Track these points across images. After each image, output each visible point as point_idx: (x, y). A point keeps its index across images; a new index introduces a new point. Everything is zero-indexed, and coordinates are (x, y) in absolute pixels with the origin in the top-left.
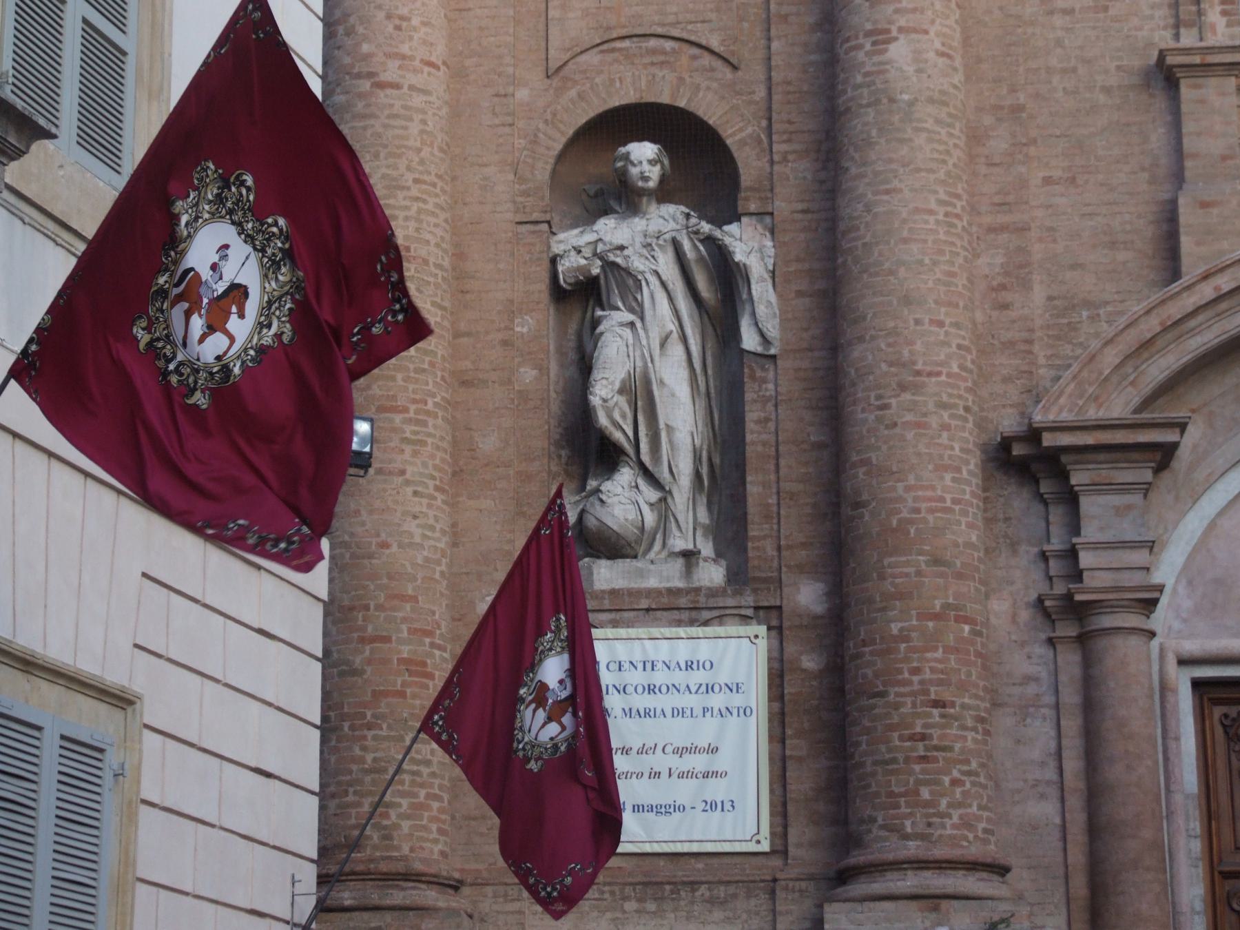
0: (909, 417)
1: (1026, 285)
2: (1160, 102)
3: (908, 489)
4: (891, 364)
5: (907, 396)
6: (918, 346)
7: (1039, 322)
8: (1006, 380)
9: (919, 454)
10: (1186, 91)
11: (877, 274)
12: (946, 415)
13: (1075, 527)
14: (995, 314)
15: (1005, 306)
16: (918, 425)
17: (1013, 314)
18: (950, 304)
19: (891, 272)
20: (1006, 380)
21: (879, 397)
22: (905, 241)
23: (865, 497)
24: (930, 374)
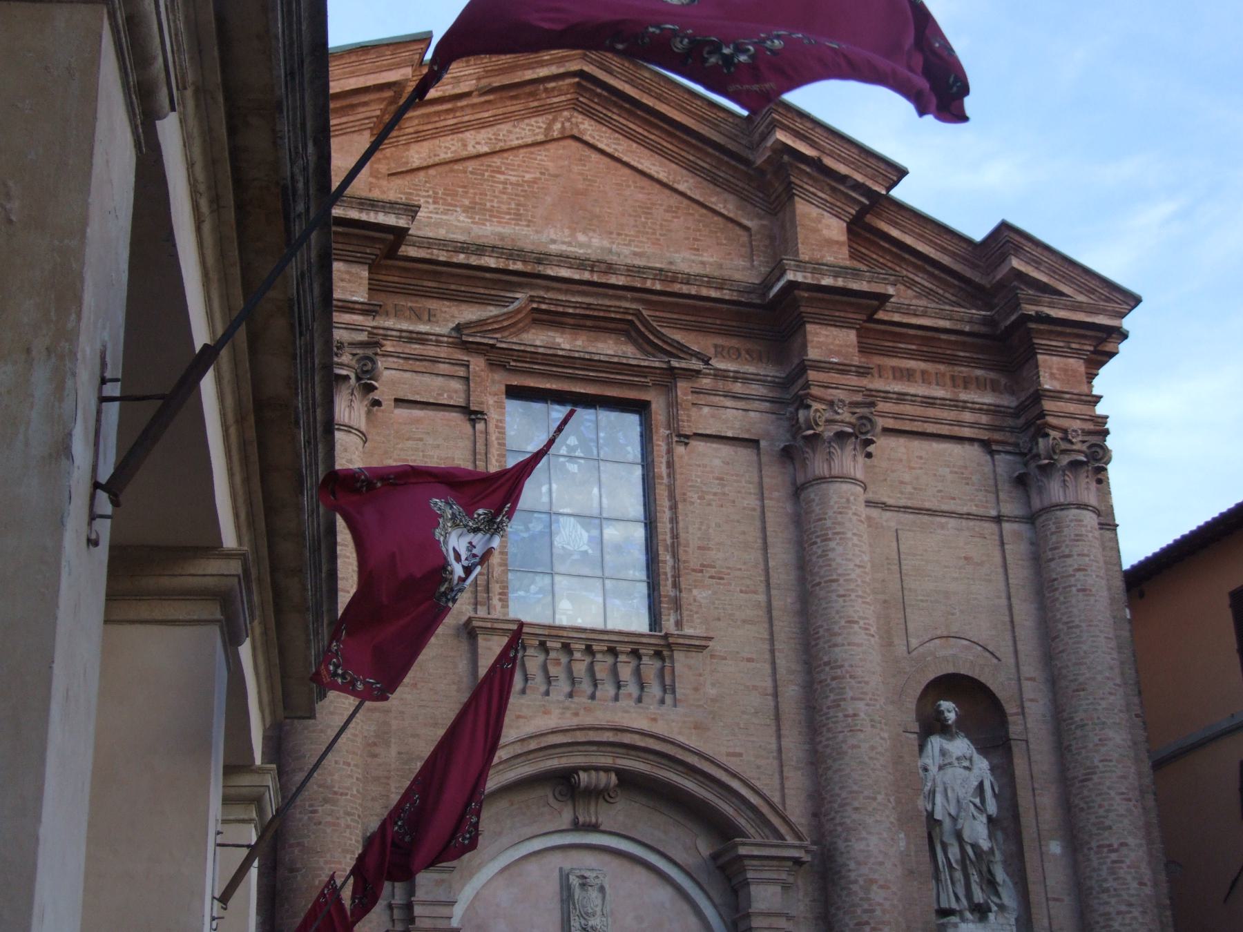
0: (329, 819)
1: (387, 744)
2: (464, 646)
3: (326, 862)
4: (320, 786)
5: (328, 807)
6: (336, 777)
7: (393, 766)
8: (373, 799)
9: (333, 842)
10: (481, 641)
11: (314, 731)
12: (349, 819)
13: (411, 892)
14: (369, 760)
15: (375, 756)
16: (334, 824)
17: (380, 761)
18: (354, 753)
19: (322, 731)
20: (373, 799)
21: (311, 806)
22: (332, 713)
23: (299, 865)
24: (342, 794)
